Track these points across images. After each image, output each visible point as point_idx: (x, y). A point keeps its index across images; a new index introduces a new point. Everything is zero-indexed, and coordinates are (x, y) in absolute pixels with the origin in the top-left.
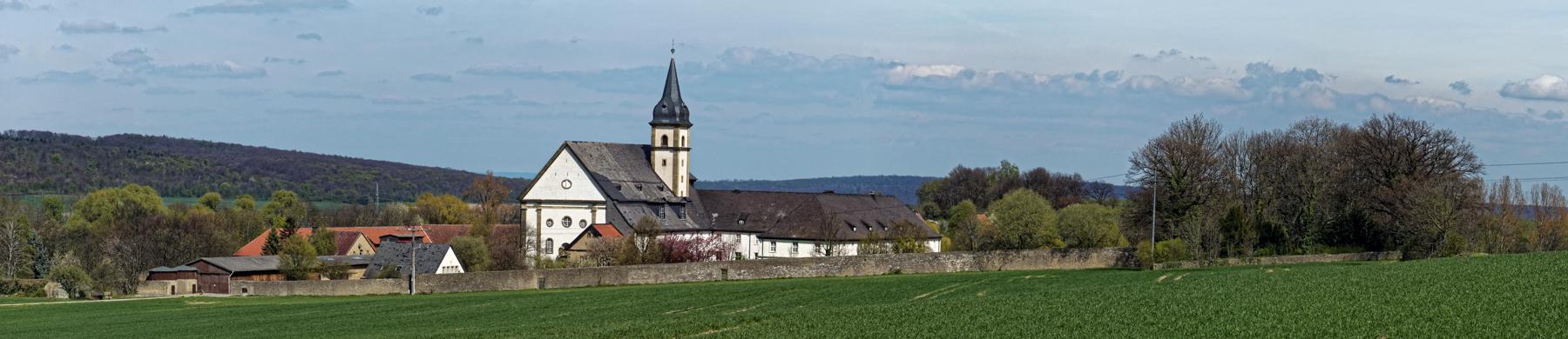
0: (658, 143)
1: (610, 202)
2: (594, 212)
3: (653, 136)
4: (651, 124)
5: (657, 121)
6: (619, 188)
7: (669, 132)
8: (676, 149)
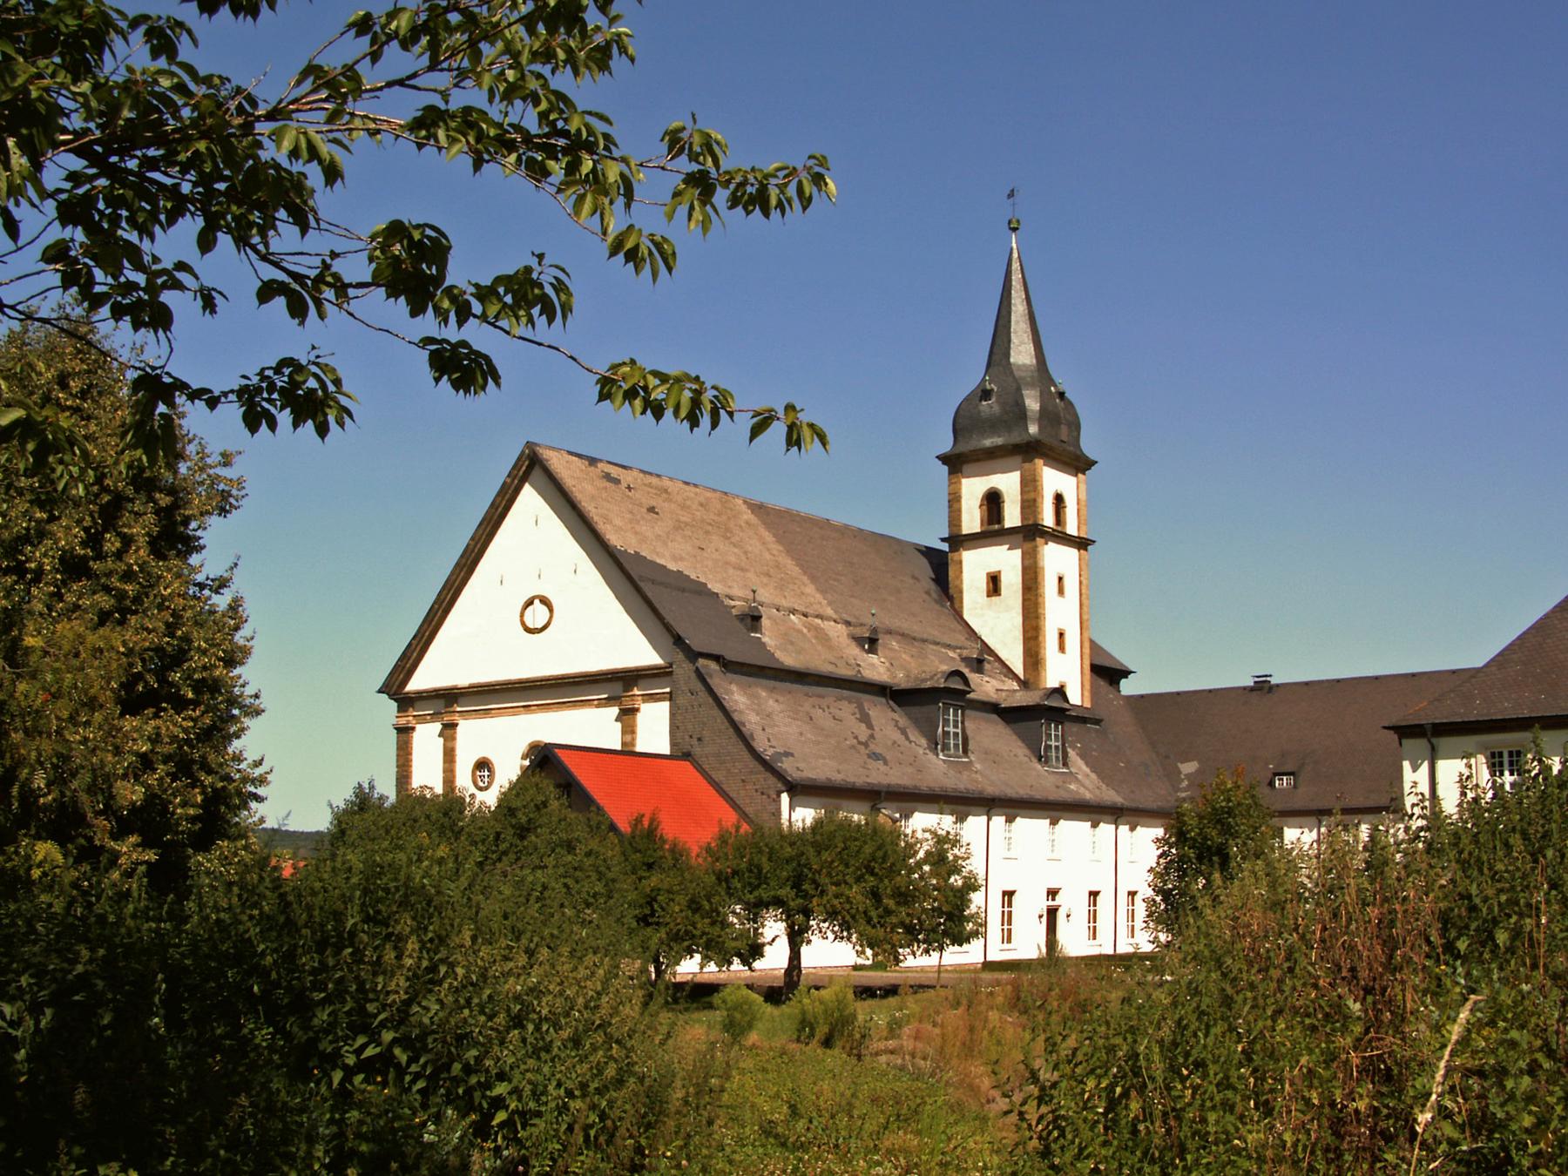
0: (972, 521)
1: (684, 669)
2: (627, 715)
3: (954, 500)
4: (945, 459)
5: (966, 447)
6: (753, 619)
7: (1008, 483)
8: (1030, 533)
